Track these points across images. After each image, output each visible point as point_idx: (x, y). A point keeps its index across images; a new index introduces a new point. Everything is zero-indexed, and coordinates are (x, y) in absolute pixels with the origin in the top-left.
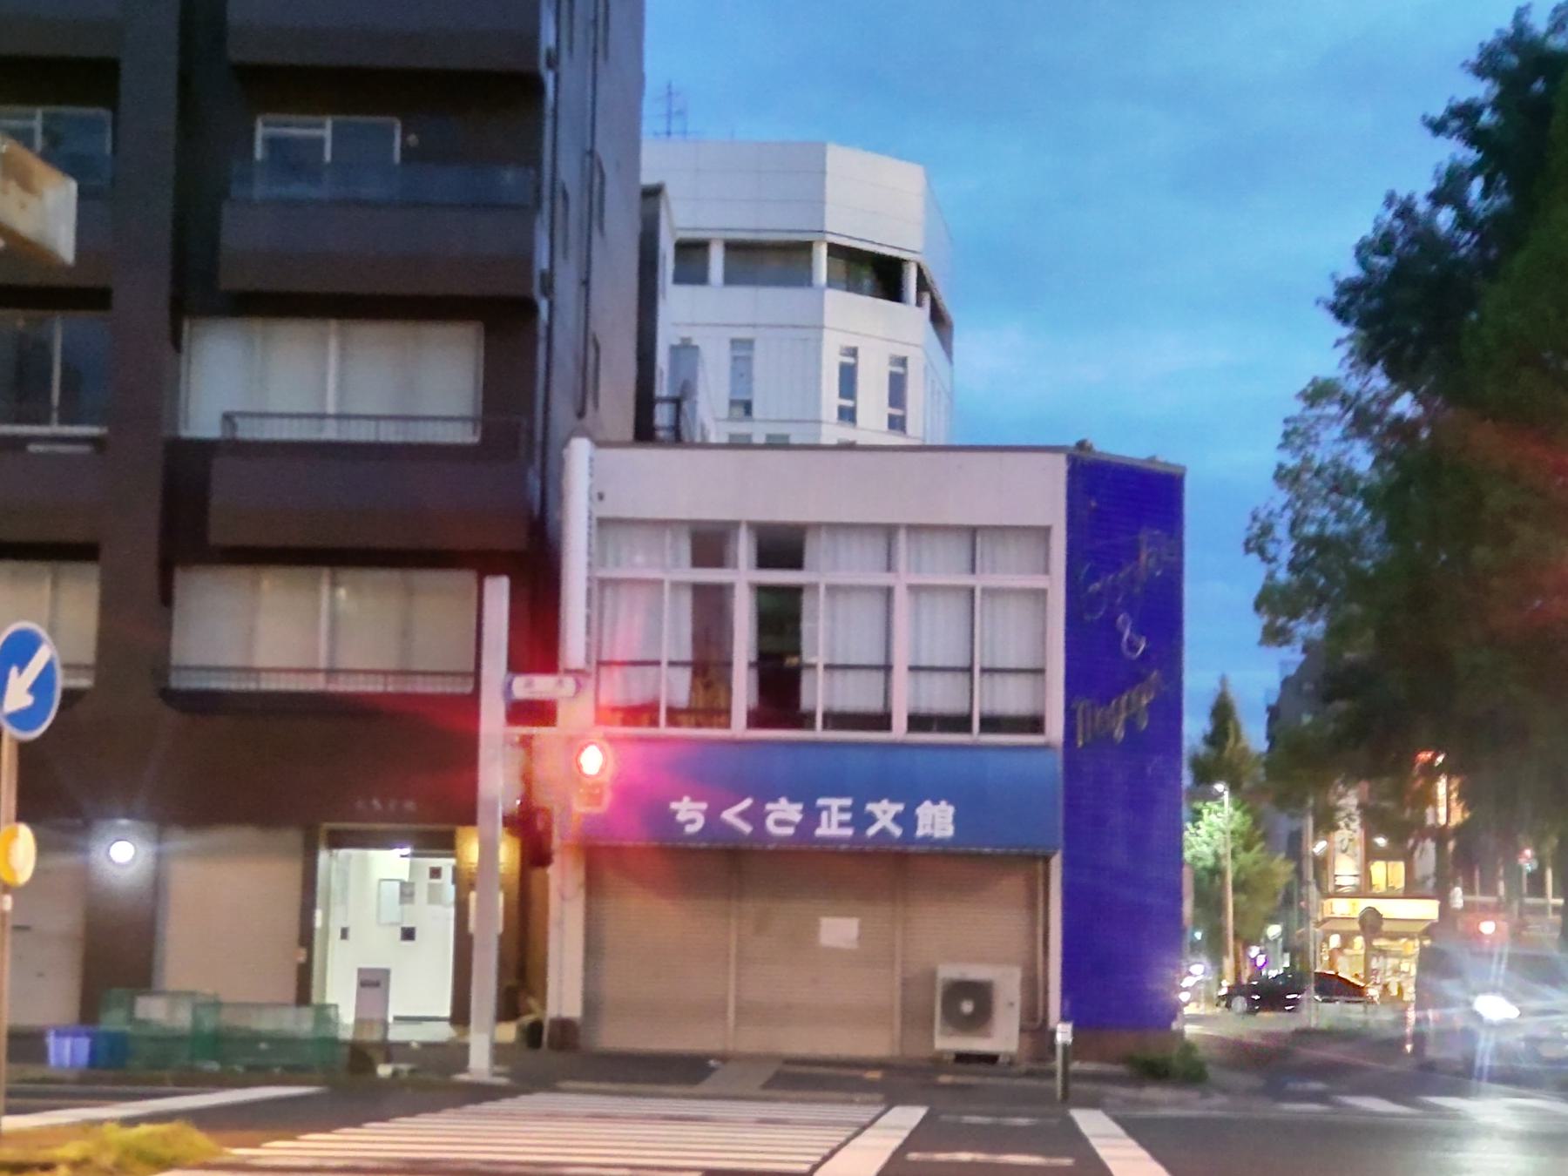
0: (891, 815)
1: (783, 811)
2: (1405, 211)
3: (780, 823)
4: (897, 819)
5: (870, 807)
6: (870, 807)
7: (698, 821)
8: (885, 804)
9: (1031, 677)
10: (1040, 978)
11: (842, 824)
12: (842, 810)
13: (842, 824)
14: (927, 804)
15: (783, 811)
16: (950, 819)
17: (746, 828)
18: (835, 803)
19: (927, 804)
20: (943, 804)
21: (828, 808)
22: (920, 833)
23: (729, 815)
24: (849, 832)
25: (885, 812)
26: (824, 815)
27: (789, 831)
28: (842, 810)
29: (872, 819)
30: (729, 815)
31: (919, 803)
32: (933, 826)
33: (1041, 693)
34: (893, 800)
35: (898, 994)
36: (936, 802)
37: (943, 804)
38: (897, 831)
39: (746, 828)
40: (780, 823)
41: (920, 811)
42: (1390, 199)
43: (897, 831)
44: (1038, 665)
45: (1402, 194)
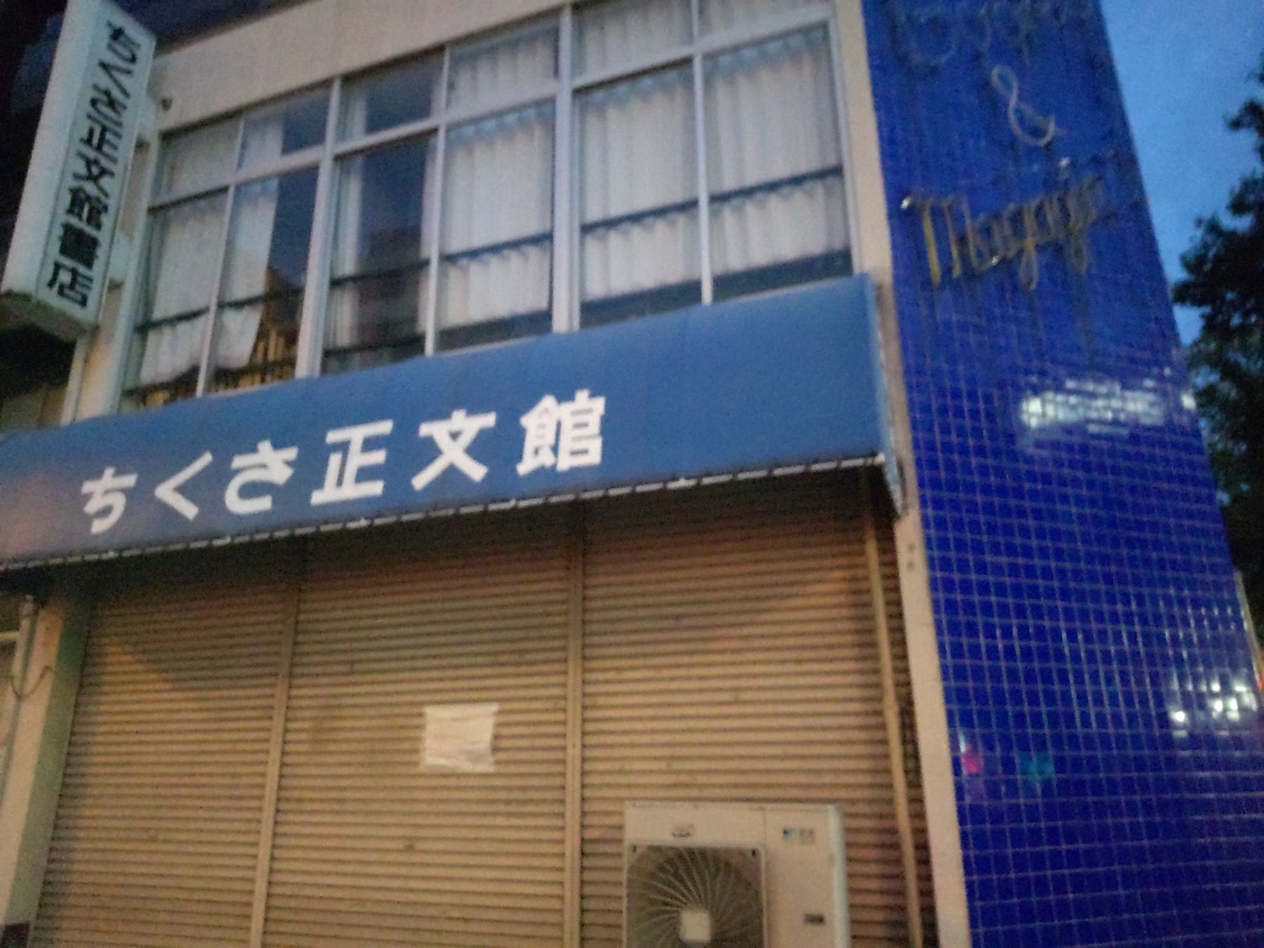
0: (467, 438)
1: (264, 466)
2: (1213, 227)
3: (249, 491)
4: (477, 449)
5: (425, 429)
6: (425, 429)
7: (115, 507)
8: (459, 419)
9: (819, 188)
10: (904, 823)
11: (364, 474)
12: (370, 444)
13: (364, 474)
14: (548, 402)
15: (264, 466)
16: (594, 423)
17: (189, 510)
18: (356, 435)
19: (548, 402)
20: (582, 396)
21: (344, 447)
22: (525, 467)
23: (166, 492)
24: (375, 488)
25: (455, 436)
26: (335, 460)
27: (264, 504)
28: (370, 444)
29: (430, 451)
30: (166, 492)
31: (531, 402)
32: (555, 449)
33: (840, 215)
34: (473, 410)
35: (570, 876)
36: (565, 396)
37: (582, 396)
38: (477, 472)
39: (189, 510)
40: (249, 491)
41: (529, 421)
42: (1199, 222)
43: (477, 472)
44: (831, 161)
45: (1207, 215)
